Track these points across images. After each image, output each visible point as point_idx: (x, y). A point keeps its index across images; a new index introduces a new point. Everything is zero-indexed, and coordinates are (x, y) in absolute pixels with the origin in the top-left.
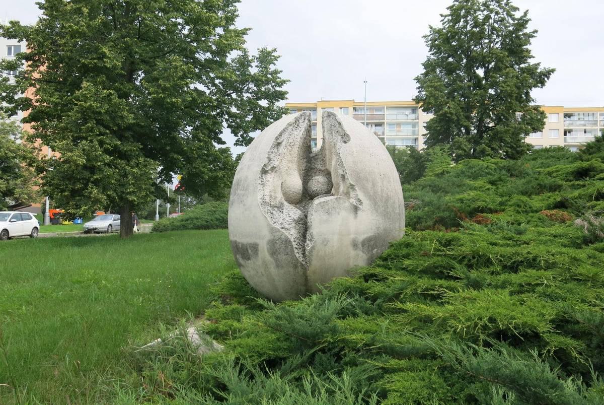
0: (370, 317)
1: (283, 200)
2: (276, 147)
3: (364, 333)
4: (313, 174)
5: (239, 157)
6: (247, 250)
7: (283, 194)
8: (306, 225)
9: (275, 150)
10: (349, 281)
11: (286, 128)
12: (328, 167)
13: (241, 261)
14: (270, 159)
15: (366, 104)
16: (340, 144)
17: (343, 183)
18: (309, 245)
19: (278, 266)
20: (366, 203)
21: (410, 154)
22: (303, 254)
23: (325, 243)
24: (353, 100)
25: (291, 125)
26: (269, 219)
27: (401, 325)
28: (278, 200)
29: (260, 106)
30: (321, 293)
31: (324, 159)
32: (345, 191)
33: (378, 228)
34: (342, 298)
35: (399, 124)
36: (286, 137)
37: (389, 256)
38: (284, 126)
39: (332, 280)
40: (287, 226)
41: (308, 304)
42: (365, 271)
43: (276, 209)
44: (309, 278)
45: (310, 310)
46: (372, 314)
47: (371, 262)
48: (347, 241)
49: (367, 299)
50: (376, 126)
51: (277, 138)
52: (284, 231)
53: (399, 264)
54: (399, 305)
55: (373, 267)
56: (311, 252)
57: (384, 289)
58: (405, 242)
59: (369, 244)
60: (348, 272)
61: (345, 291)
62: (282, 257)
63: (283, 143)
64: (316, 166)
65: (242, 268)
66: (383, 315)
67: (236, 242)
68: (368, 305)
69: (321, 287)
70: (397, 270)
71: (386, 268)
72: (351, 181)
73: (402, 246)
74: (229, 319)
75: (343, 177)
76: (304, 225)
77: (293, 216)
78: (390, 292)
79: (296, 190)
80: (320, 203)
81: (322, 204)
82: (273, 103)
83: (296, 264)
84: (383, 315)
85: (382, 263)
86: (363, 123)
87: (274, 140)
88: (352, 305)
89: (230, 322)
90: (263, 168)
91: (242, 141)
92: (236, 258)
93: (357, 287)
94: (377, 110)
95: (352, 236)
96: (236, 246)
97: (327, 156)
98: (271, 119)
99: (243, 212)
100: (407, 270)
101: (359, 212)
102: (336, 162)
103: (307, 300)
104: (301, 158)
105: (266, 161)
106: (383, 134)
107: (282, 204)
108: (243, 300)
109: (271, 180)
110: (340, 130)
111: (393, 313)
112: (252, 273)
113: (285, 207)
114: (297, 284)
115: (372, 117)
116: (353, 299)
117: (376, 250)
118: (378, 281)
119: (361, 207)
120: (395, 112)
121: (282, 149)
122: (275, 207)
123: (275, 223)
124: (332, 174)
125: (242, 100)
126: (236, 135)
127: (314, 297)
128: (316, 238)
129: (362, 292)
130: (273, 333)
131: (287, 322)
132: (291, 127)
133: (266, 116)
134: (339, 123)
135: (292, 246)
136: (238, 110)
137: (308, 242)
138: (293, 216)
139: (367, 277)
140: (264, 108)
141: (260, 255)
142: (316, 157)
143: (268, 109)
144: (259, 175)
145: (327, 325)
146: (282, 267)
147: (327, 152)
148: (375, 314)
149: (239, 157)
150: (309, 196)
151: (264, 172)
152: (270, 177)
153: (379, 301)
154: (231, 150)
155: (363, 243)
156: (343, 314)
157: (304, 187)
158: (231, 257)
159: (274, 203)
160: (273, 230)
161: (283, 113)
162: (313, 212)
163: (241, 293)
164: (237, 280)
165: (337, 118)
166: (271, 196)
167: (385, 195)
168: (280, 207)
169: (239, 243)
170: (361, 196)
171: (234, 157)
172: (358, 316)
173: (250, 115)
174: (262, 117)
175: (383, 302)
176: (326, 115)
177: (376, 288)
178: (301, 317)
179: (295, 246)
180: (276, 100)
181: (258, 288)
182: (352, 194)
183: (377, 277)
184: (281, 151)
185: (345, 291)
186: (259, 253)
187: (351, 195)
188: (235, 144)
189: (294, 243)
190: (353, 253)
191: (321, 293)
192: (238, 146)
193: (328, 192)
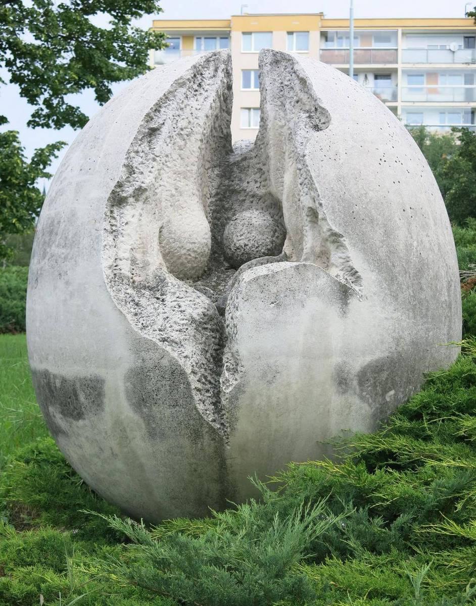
0: (383, 558)
1: (165, 269)
2: (146, 140)
3: (370, 597)
4: (236, 206)
5: (42, 158)
6: (76, 395)
7: (165, 256)
8: (221, 334)
9: (145, 146)
10: (332, 471)
11: (170, 92)
12: (273, 189)
13: (60, 420)
14: (130, 170)
15: (353, 24)
16: (303, 132)
17: (313, 228)
18: (229, 382)
19: (152, 434)
20: (370, 279)
21: (460, 147)
22: (214, 404)
23: (269, 377)
24: (321, 14)
25: (182, 85)
26: (129, 317)
27: (458, 575)
28: (152, 269)
29: (92, 28)
30: (260, 500)
31: (264, 168)
32: (318, 249)
33: (397, 341)
34: (314, 514)
35: (432, 75)
36: (170, 113)
37: (425, 406)
38: (167, 87)
39: (286, 469)
40: (175, 336)
41: (229, 528)
42: (368, 445)
43: (147, 293)
44: (228, 462)
45: (237, 544)
46: (388, 551)
47: (381, 422)
48: (324, 372)
49: (372, 513)
50: (376, 77)
51: (149, 118)
52: (169, 349)
53: (450, 428)
54: (455, 529)
55: (386, 436)
56: (234, 398)
57: (415, 488)
58: (462, 372)
59: (376, 377)
60: (327, 448)
61: (321, 494)
62: (163, 412)
63: (165, 130)
64: (245, 184)
65: (62, 440)
66: (413, 553)
67: (46, 374)
68: (377, 529)
69: (260, 485)
70: (443, 442)
71: (417, 437)
72: (332, 224)
73: (456, 384)
74: (31, 564)
75: (314, 214)
76: (216, 333)
77: (189, 311)
78: (429, 496)
79: (195, 247)
80: (256, 279)
81: (262, 281)
82: (126, 22)
83: (196, 429)
84: (413, 553)
85: (407, 424)
86: (346, 71)
87: (139, 121)
88: (337, 529)
89: (36, 572)
90: (113, 192)
91: (48, 116)
92: (47, 414)
93: (350, 485)
94: (380, 38)
95: (336, 360)
96: (48, 384)
97: (272, 162)
98: (121, 59)
99: (65, 300)
100: (468, 443)
101: (353, 302)
102: (295, 176)
103: (226, 517)
104: (208, 165)
105: (121, 174)
106: (395, 97)
107: (162, 281)
108: (65, 517)
109: (135, 220)
110: (304, 97)
111: (439, 548)
112: (89, 450)
113: (170, 289)
114: (200, 477)
115: (368, 57)
116: (341, 516)
117: (392, 392)
118: (398, 468)
119: (357, 288)
120: (424, 43)
121: (160, 144)
122: (145, 287)
123: (144, 327)
124: (285, 205)
125: (47, 13)
126: (32, 100)
127: (245, 511)
128: (246, 364)
129: (362, 498)
130: (147, 599)
131: (183, 576)
132: (183, 90)
133: (108, 52)
134: (303, 81)
135: (189, 384)
136: (37, 38)
137: (227, 374)
138: (189, 311)
139: (374, 460)
140: (103, 33)
142: (245, 163)
143: (112, 36)
144: (104, 208)
145: (280, 581)
146: (163, 435)
147: (272, 152)
148: (395, 552)
149: (42, 158)
150: (228, 259)
151: (117, 200)
152: (130, 213)
153: (402, 519)
154: (20, 137)
155: (363, 377)
156: (317, 553)
157: (214, 238)
158: (32, 406)
160: (139, 346)
161: (150, 46)
162: (239, 301)
163: (59, 500)
164: (47, 468)
165: (296, 67)
166: (134, 261)
167: (414, 259)
168: (156, 289)
169: (55, 376)
170: (358, 262)
171: (28, 156)
172: (352, 555)
173: (66, 51)
174: (97, 55)
175: (414, 520)
176: (269, 59)
177: (396, 486)
178: (217, 561)
179: (195, 384)
180: (133, 14)
181: (102, 488)
182: (336, 256)
183: (394, 459)
184: (157, 151)
185: (321, 494)
186: (106, 400)
188: (29, 123)
189: (192, 378)
190: (336, 401)
191: (260, 500)
192: (38, 129)
193: (274, 251)
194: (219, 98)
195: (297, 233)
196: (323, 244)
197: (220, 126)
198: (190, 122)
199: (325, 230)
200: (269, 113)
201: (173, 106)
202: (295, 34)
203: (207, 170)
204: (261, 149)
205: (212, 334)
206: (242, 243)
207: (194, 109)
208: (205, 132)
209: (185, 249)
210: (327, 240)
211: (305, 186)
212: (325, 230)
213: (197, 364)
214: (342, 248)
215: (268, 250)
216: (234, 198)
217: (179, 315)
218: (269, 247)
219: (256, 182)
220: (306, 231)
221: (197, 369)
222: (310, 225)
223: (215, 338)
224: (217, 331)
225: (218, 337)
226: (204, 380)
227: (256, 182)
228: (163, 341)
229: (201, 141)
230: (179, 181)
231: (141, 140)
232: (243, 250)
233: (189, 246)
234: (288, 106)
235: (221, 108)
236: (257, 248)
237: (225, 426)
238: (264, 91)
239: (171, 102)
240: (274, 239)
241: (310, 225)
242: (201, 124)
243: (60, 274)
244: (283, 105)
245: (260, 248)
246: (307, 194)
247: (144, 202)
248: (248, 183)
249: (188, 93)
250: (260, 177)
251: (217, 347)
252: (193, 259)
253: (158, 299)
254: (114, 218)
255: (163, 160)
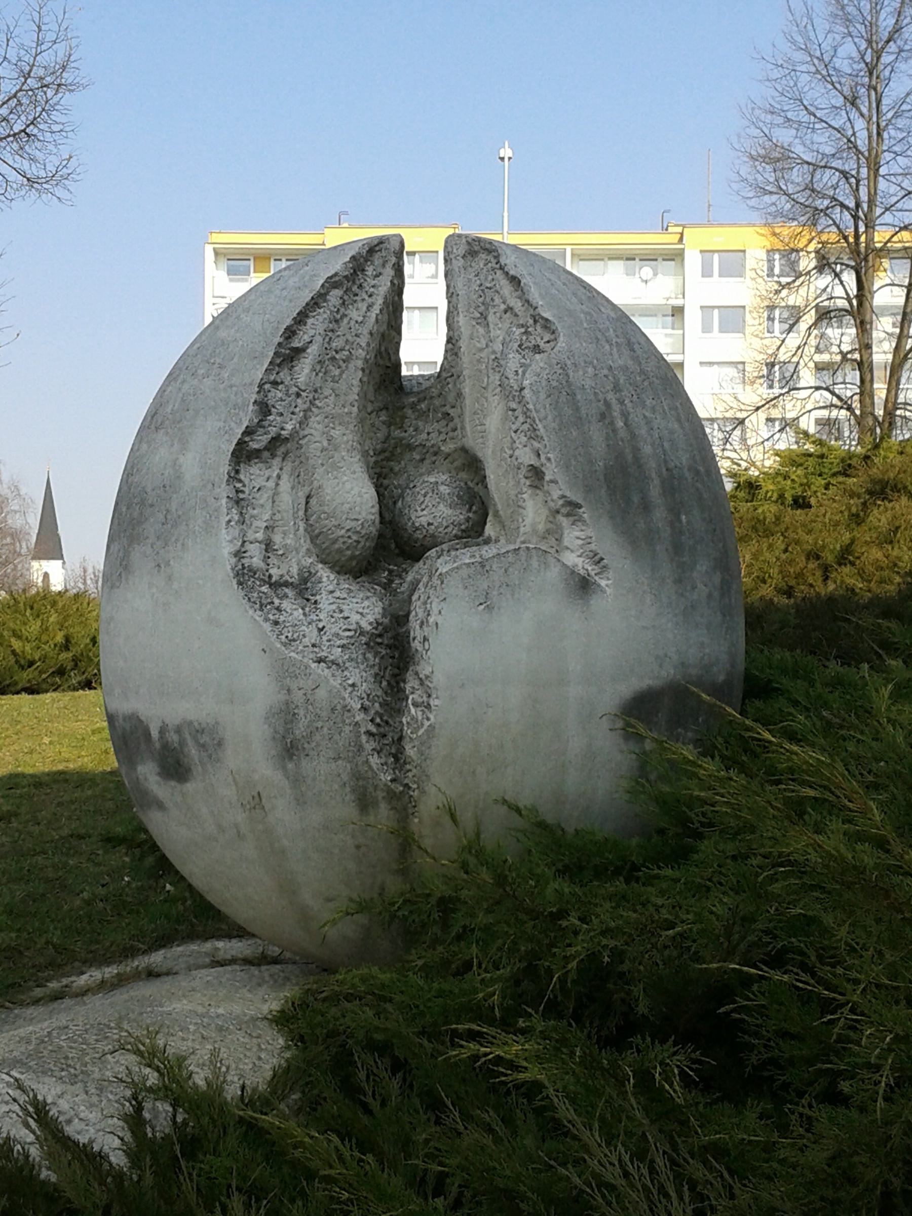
12: (470, 442)
14: (264, 409)
32: (541, 527)
51: (290, 333)
63: (313, 350)
76: (393, 650)
102: (505, 419)
105: (248, 416)
132: (337, 292)
141: (232, 759)
159: (283, 571)
168: (304, 588)
187: (566, 542)
194: (388, 307)
195: (508, 505)
196: (551, 519)
197: (386, 350)
198: (347, 340)
199: (555, 497)
200: (462, 329)
201: (325, 316)
202: (417, 255)
203: (369, 414)
204: (448, 384)
205: (388, 651)
206: (424, 521)
207: (352, 323)
208: (368, 357)
209: (343, 528)
210: (558, 512)
211: (523, 434)
212: (555, 497)
213: (368, 695)
214: (580, 524)
215: (463, 531)
216: (407, 456)
217: (342, 624)
218: (463, 527)
219: (440, 433)
220: (524, 501)
221: (367, 703)
222: (529, 492)
223: (393, 657)
224: (396, 647)
225: (397, 656)
226: (378, 720)
227: (440, 433)
228: (319, 663)
229: (363, 370)
230: (333, 428)
231: (279, 365)
232: (424, 531)
233: (349, 524)
234: (491, 318)
235: (389, 323)
236: (446, 527)
237: (410, 788)
238: (454, 296)
239: (322, 310)
240: (471, 515)
241: (529, 492)
242: (364, 345)
243: (159, 566)
244: (484, 316)
245: (450, 529)
246: (525, 446)
247: (283, 459)
248: (428, 434)
249: (346, 297)
250: (447, 425)
251: (396, 671)
252: (355, 544)
253: (308, 600)
254: (240, 481)
255: (311, 396)
